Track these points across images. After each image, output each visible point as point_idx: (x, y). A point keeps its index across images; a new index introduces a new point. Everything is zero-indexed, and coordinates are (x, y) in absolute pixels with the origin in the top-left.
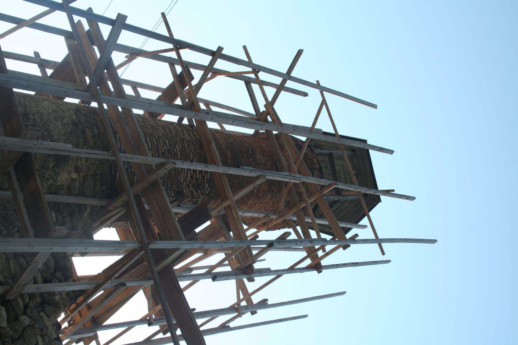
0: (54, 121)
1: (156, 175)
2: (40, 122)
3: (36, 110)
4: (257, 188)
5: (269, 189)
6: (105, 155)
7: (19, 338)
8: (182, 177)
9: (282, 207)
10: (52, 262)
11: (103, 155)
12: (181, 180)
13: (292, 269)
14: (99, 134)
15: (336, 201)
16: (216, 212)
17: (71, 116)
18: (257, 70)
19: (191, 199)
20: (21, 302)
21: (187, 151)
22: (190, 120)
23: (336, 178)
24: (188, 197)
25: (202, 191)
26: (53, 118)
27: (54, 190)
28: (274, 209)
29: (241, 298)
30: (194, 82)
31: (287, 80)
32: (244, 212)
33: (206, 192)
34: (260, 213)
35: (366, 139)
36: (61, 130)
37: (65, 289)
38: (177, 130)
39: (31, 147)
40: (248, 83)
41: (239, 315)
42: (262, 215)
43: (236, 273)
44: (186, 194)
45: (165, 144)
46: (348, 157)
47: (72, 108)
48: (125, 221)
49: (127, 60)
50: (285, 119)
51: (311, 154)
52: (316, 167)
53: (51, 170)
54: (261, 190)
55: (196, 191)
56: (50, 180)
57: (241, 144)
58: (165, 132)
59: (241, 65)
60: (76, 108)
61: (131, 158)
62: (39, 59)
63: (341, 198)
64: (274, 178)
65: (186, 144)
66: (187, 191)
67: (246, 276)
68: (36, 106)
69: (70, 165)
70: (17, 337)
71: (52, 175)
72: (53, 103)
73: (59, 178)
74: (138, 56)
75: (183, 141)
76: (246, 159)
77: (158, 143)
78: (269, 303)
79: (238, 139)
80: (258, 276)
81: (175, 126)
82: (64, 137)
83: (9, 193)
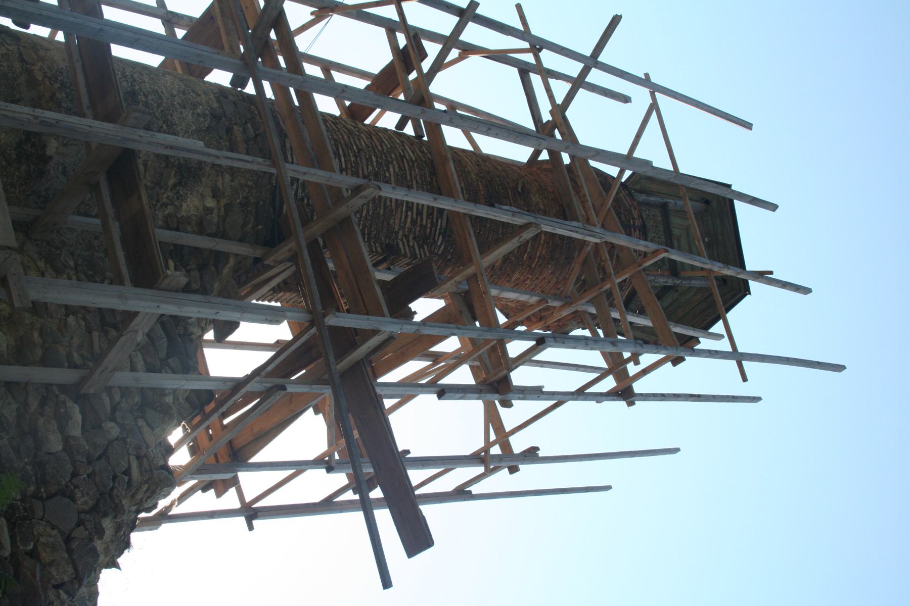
0: (179, 109)
1: (347, 206)
2: (155, 108)
3: (150, 88)
4: (529, 252)
5: (550, 256)
6: (259, 164)
7: (99, 458)
8: (397, 222)
9: (571, 288)
10: (163, 341)
11: (257, 164)
12: (394, 226)
13: (581, 394)
14: (257, 136)
15: (670, 286)
16: (451, 284)
17: (211, 102)
18: (537, 47)
19: (410, 260)
20: (107, 400)
21: (408, 176)
22: (417, 127)
23: (670, 242)
24: (405, 256)
25: (431, 249)
26: (179, 104)
27: (176, 224)
28: (558, 292)
29: (491, 440)
30: (426, 65)
31: (591, 68)
32: (503, 290)
33: (438, 251)
34: (532, 295)
35: (731, 184)
36: (192, 124)
37: (182, 386)
38: (392, 141)
39: (134, 141)
40: (524, 71)
41: (488, 472)
42: (534, 299)
43: (480, 388)
44: (403, 251)
45: (369, 163)
46: (694, 213)
47: (212, 90)
48: (296, 292)
49: (314, 19)
50: (585, 138)
51: (629, 202)
52: (637, 225)
53: (171, 190)
54: (536, 254)
55: (421, 247)
56: (169, 207)
57: (504, 174)
58: (371, 143)
59: (509, 36)
60: (220, 90)
61: (305, 174)
62: (163, 11)
63: (678, 282)
64: (554, 229)
65: (406, 166)
66: (404, 245)
67: (497, 395)
68: (150, 82)
69: (203, 184)
70: (97, 455)
71: (173, 198)
72: (181, 80)
73: (184, 205)
74: (331, 12)
75: (402, 159)
76: (512, 201)
77: (358, 159)
78: (541, 454)
79: (501, 166)
80: (519, 399)
81: (390, 135)
82: (195, 135)
83: (97, 221)
